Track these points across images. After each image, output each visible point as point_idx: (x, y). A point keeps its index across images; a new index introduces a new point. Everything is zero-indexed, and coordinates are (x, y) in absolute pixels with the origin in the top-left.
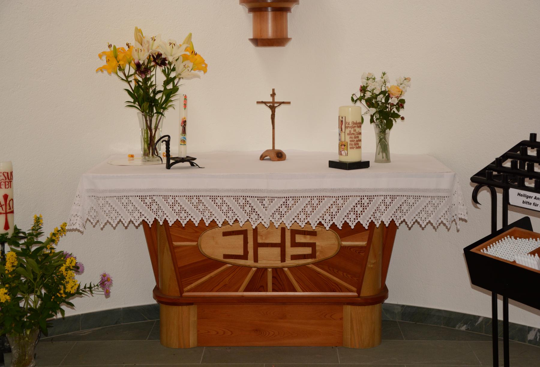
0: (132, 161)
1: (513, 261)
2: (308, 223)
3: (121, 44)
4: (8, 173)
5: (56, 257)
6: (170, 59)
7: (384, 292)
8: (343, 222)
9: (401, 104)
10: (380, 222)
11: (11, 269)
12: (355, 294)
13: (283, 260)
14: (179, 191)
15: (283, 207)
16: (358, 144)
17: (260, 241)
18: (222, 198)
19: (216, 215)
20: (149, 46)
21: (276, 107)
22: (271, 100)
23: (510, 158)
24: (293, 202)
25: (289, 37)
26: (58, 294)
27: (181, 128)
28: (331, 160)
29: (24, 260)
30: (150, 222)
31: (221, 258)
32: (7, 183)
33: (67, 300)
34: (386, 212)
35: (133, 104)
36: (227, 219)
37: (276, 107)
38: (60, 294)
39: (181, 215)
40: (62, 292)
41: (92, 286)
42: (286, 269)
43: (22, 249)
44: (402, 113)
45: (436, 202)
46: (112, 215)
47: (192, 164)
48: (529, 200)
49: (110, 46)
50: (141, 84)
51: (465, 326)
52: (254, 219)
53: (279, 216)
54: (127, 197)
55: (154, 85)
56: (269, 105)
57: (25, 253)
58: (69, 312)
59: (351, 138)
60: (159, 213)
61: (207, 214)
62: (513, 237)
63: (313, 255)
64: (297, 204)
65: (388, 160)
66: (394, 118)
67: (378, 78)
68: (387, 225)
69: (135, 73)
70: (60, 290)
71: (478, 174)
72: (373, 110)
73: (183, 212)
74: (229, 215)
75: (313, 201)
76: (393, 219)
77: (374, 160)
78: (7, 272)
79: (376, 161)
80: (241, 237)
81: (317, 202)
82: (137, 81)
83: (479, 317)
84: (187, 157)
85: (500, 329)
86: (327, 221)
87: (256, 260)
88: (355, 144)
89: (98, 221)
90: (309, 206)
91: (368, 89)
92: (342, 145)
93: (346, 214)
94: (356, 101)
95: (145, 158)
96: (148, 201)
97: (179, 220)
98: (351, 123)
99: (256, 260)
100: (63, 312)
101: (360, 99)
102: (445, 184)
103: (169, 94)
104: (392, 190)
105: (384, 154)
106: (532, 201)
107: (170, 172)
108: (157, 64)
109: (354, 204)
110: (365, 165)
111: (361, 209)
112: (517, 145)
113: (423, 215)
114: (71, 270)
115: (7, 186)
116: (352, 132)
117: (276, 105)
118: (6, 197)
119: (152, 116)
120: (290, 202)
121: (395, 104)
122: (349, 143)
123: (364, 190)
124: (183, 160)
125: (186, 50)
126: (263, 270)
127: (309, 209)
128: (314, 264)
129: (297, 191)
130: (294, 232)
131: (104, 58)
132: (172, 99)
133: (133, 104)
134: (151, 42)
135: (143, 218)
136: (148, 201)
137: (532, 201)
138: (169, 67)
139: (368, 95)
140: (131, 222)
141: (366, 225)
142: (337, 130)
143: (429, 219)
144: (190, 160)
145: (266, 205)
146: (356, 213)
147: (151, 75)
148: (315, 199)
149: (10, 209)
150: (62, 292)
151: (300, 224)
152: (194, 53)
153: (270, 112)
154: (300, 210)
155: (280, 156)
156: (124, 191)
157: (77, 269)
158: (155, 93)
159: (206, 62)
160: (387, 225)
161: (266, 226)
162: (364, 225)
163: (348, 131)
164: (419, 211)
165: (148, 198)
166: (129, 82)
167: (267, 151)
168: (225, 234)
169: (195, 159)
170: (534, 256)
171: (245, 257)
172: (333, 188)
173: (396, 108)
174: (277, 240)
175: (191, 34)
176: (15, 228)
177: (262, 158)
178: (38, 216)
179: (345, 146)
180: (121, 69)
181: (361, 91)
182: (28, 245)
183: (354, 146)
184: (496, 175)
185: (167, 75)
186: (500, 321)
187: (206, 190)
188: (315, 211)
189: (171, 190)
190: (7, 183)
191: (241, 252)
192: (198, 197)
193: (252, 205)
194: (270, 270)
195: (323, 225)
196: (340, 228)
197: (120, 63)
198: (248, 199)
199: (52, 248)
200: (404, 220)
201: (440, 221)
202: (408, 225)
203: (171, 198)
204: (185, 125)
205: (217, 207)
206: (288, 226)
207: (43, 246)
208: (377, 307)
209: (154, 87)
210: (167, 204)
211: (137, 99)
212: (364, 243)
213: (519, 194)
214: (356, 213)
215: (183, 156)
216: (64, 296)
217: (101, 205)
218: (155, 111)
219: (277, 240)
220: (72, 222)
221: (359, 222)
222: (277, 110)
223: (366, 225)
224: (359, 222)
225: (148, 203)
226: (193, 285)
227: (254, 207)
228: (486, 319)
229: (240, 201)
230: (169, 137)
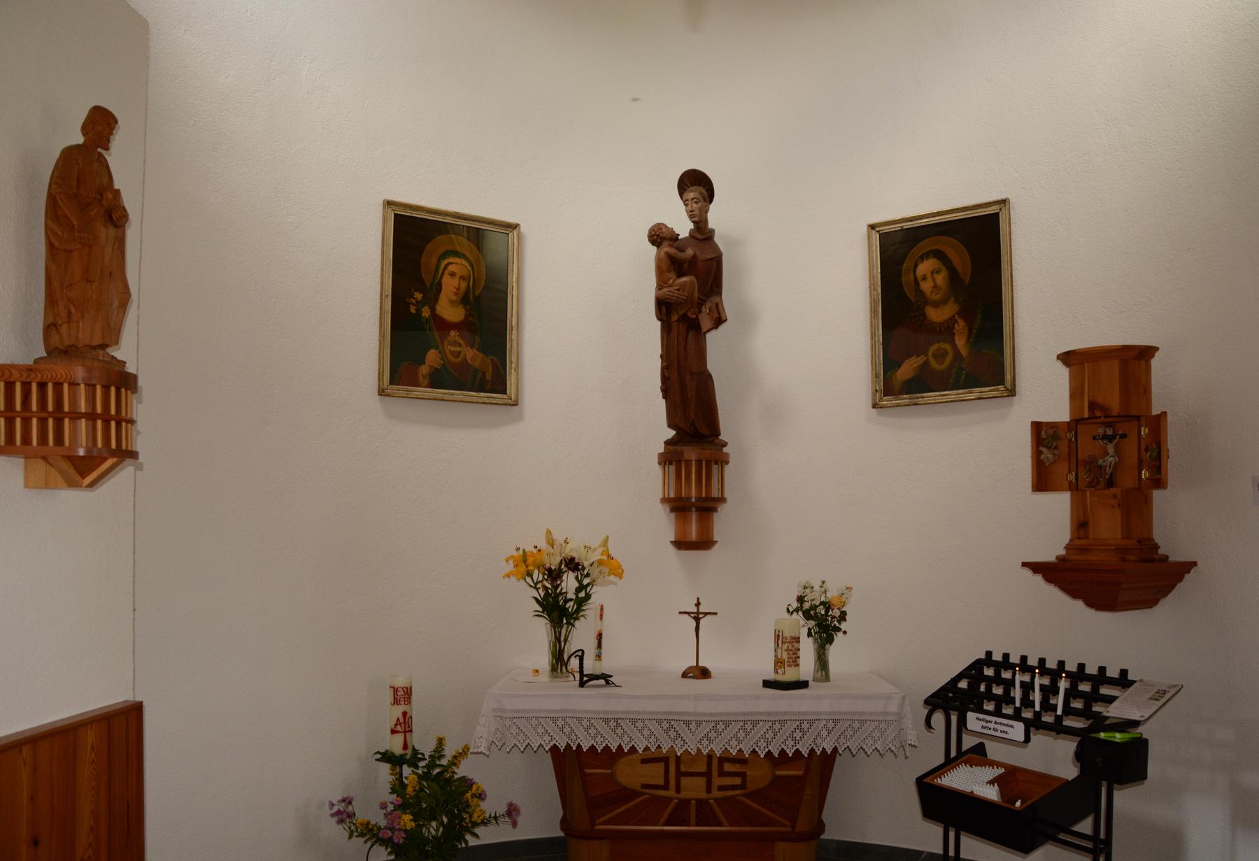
0: (536, 678)
1: (969, 791)
4: (407, 688)
6: (586, 564)
7: (821, 827)
9: (843, 616)
10: (821, 750)
11: (413, 794)
12: (789, 829)
13: (709, 790)
16: (796, 661)
17: (683, 769)
18: (643, 721)
20: (561, 550)
21: (701, 618)
22: (695, 610)
23: (966, 678)
25: (715, 539)
26: (463, 823)
27: (596, 641)
29: (425, 784)
30: (562, 746)
31: (638, 788)
33: (471, 829)
34: (828, 738)
37: (701, 618)
40: (467, 821)
41: (498, 815)
42: (712, 801)
44: (843, 626)
45: (883, 726)
46: (520, 738)
47: (608, 682)
48: (989, 725)
49: (518, 549)
52: (679, 746)
54: (537, 718)
55: (564, 593)
56: (692, 615)
57: (426, 776)
58: (472, 842)
61: (626, 739)
63: (742, 786)
64: (728, 729)
65: (827, 679)
66: (835, 632)
68: (829, 753)
71: (933, 695)
72: (812, 623)
76: (836, 746)
78: (408, 796)
80: (662, 765)
81: (751, 726)
82: (546, 588)
84: (603, 674)
86: (762, 748)
87: (678, 790)
88: (793, 662)
89: (504, 744)
90: (741, 731)
92: (779, 663)
93: (783, 740)
94: (792, 613)
95: (552, 674)
96: (560, 723)
97: (595, 745)
99: (678, 790)
100: (466, 842)
101: (797, 610)
102: (893, 707)
103: (581, 602)
104: (835, 713)
105: (824, 673)
106: (991, 725)
107: (584, 691)
108: (570, 569)
110: (803, 685)
111: (800, 735)
112: (973, 663)
113: (869, 741)
115: (406, 703)
117: (700, 616)
118: (405, 714)
119: (562, 628)
120: (721, 727)
121: (837, 616)
124: (597, 677)
125: (602, 554)
126: (687, 802)
128: (744, 795)
130: (722, 760)
131: (511, 562)
132: (584, 608)
135: (555, 742)
136: (560, 723)
137: (991, 725)
138: (582, 572)
139: (806, 606)
140: (541, 745)
141: (805, 752)
142: (772, 645)
143: (876, 746)
144: (606, 677)
150: (467, 821)
151: (731, 751)
152: (609, 556)
153: (694, 624)
154: (732, 735)
155: (704, 673)
156: (533, 711)
157: (481, 796)
158: (567, 601)
159: (623, 567)
160: (829, 753)
161: (693, 753)
162: (803, 753)
163: (785, 646)
164: (864, 736)
166: (537, 589)
167: (690, 667)
168: (644, 761)
169: (611, 676)
170: (994, 785)
171: (666, 787)
172: (768, 710)
175: (608, 537)
176: (414, 748)
177: (685, 675)
178: (441, 737)
179: (781, 663)
180: (530, 574)
181: (798, 601)
183: (791, 664)
185: (580, 582)
187: (626, 712)
189: (586, 712)
191: (661, 782)
192: (616, 720)
193: (677, 729)
194: (693, 802)
195: (757, 752)
196: (777, 756)
198: (673, 723)
199: (454, 772)
200: (848, 747)
201: (887, 748)
202: (852, 753)
203: (586, 720)
204: (601, 638)
207: (445, 769)
210: (581, 727)
211: (546, 607)
212: (801, 773)
213: (978, 719)
214: (794, 739)
215: (598, 672)
217: (508, 726)
218: (565, 621)
222: (702, 621)
223: (805, 752)
225: (560, 726)
226: (605, 818)
227: (680, 732)
230: (583, 651)
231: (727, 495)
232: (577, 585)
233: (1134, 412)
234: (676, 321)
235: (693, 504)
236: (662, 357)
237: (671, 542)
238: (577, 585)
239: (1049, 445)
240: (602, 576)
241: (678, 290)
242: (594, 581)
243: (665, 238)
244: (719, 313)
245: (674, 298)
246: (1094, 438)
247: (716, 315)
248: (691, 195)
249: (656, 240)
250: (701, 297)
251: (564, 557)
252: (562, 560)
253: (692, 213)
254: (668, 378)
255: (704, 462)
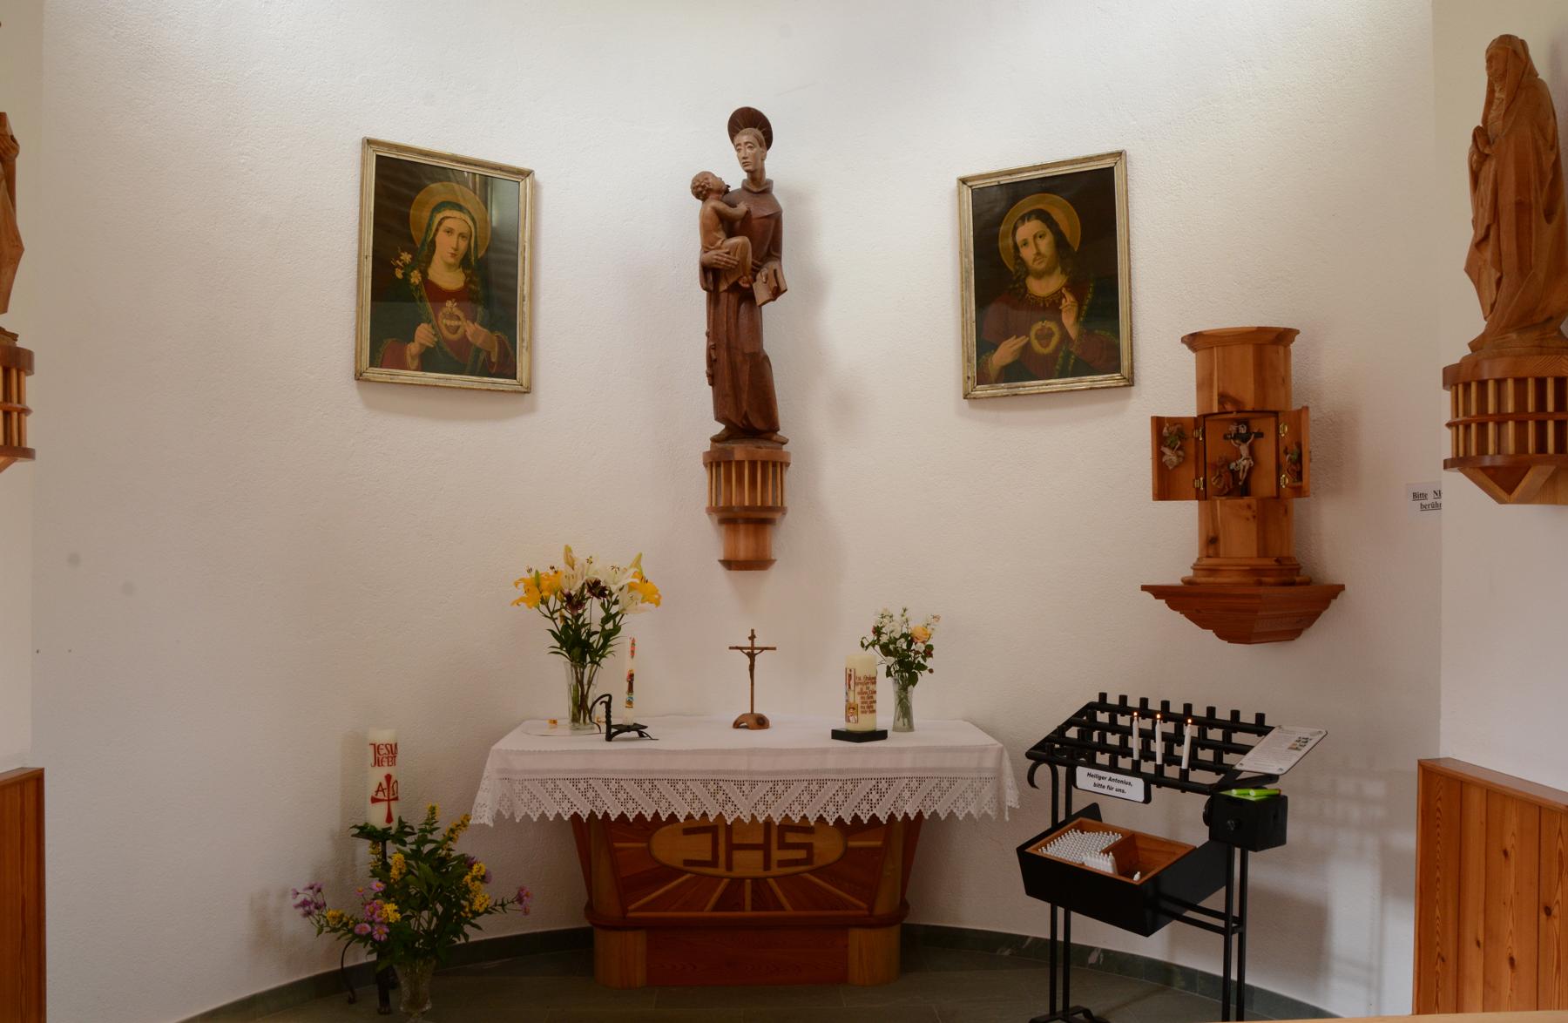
2: (804, 818)
3: (544, 569)
4: (391, 745)
5: (455, 863)
6: (614, 588)
8: (853, 815)
9: (928, 652)
10: (902, 815)
12: (867, 913)
13: (767, 866)
14: (625, 772)
15: (770, 794)
16: (872, 707)
18: (685, 781)
19: (676, 806)
22: (748, 644)
24: (783, 788)
25: (773, 558)
28: (834, 728)
31: (679, 865)
32: (390, 759)
33: (473, 921)
35: (559, 650)
36: (692, 813)
38: (464, 912)
39: (628, 806)
40: (467, 910)
41: (506, 902)
43: (411, 850)
47: (641, 735)
48: (1102, 782)
49: (530, 571)
50: (570, 623)
51: (1009, 950)
53: (764, 808)
55: (587, 624)
56: (746, 651)
57: (416, 854)
58: (474, 936)
59: (862, 698)
60: (596, 803)
61: (664, 804)
62: (1078, 831)
63: (808, 860)
64: (789, 790)
65: (910, 728)
67: (897, 617)
69: (562, 607)
70: (465, 907)
71: (1035, 748)
72: (892, 660)
73: (631, 802)
74: (694, 806)
75: (811, 786)
77: (891, 729)
78: (392, 881)
79: (895, 729)
80: (708, 836)
81: (817, 787)
82: (564, 619)
83: (1027, 937)
84: (635, 724)
85: (1060, 953)
86: (831, 813)
87: (729, 867)
88: (868, 707)
91: (884, 630)
92: (851, 709)
93: (856, 804)
94: (867, 647)
96: (582, 785)
98: (862, 678)
100: (466, 936)
101: (873, 644)
103: (607, 636)
105: (906, 720)
106: (1105, 783)
108: (594, 595)
109: (868, 790)
110: (881, 735)
114: (478, 880)
115: (390, 763)
116: (864, 690)
117: (756, 652)
118: (388, 778)
119: (584, 667)
120: (780, 788)
122: (860, 705)
123: (881, 771)
124: (628, 729)
125: (634, 575)
126: (738, 882)
127: (806, 797)
128: (810, 872)
129: (789, 772)
131: (521, 586)
133: (559, 650)
134: (587, 565)
135: (575, 810)
137: (1105, 783)
139: (884, 639)
141: (883, 819)
144: (639, 729)
145: (746, 792)
146: (870, 802)
147: (612, 622)
148: (814, 783)
149: (394, 794)
150: (467, 910)
153: (747, 661)
155: (761, 723)
158: (590, 634)
159: (659, 592)
162: (881, 819)
163: (858, 689)
165: (582, 781)
166: (554, 620)
169: (645, 727)
170: (1108, 855)
171: (714, 863)
173: (922, 657)
174: (760, 840)
175: (641, 555)
179: (854, 709)
180: (544, 601)
181: (874, 633)
182: (422, 841)
184: (1058, 749)
185: (607, 610)
186: (1060, 942)
187: (663, 772)
188: (813, 800)
190: (390, 759)
191: (708, 857)
192: (651, 781)
196: (849, 823)
197: (543, 594)
203: (614, 782)
204: (632, 680)
205: (678, 795)
206: (777, 820)
208: (896, 930)
209: (588, 627)
210: (609, 791)
214: (870, 802)
215: (630, 723)
216: (470, 915)
218: (588, 659)
219: (760, 840)
220: (478, 814)
221: (874, 814)
223: (883, 819)
224: (874, 814)
227: (730, 795)
228: (1037, 940)
229: (709, 787)
233: (1270, 407)
239: (1173, 445)
246: (1225, 437)
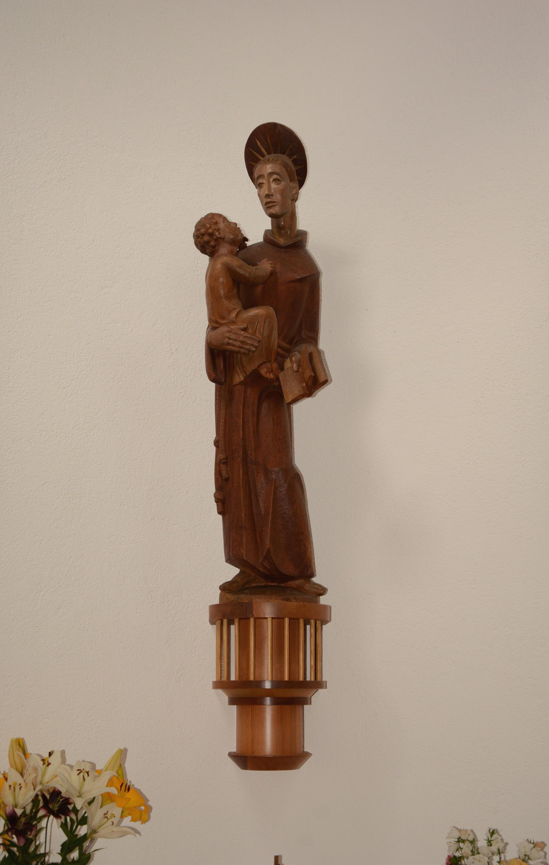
6: (79, 803)
108: (50, 812)
125: (110, 783)
231: (326, 677)
232: (64, 838)
234: (241, 383)
235: (268, 693)
236: (216, 443)
237: (231, 755)
238: (64, 838)
240: (110, 822)
241: (245, 330)
242: (94, 831)
243: (223, 239)
244: (314, 369)
245: (238, 344)
247: (308, 373)
248: (269, 168)
249: (208, 243)
250: (284, 344)
251: (41, 791)
252: (37, 796)
253: (269, 200)
254: (227, 480)
255: (287, 621)
